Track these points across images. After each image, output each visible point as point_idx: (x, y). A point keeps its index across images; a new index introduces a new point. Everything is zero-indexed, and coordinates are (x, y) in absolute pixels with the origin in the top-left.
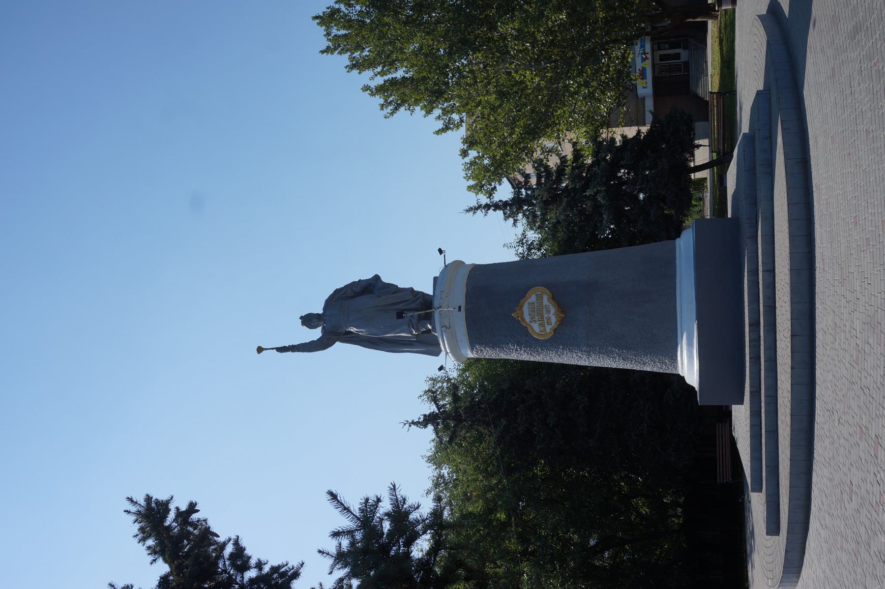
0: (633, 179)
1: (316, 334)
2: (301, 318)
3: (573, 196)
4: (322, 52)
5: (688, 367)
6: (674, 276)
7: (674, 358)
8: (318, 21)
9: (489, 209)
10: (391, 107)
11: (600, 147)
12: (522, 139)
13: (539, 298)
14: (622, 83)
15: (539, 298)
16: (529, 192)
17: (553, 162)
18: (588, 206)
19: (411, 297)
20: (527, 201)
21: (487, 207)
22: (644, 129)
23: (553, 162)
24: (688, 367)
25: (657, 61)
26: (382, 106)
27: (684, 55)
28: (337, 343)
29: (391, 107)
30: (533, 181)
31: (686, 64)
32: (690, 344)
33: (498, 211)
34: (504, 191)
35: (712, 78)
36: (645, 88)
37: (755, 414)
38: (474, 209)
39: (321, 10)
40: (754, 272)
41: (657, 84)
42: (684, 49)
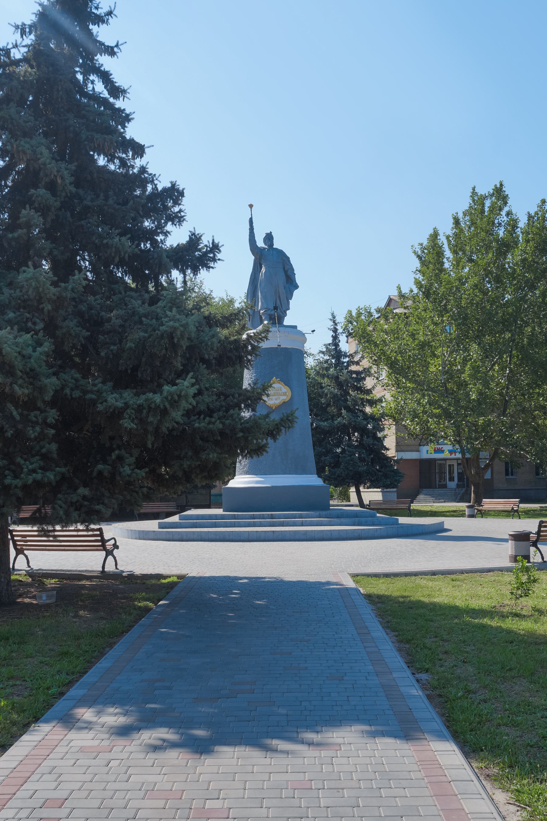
0: (353, 445)
1: (260, 243)
2: (271, 233)
3: (340, 400)
4: (474, 189)
5: (240, 481)
6: (296, 473)
7: (248, 473)
8: (498, 186)
9: (333, 331)
10: (419, 253)
11: (376, 420)
12: (388, 358)
13: (285, 394)
14: (427, 436)
15: (285, 394)
16: (345, 364)
17: (369, 383)
18: (333, 410)
19: (284, 309)
20: (339, 363)
21: (335, 330)
22: (391, 453)
23: (369, 383)
24: (240, 481)
25: (448, 463)
26: (422, 244)
27: (452, 485)
28: (254, 257)
29: (419, 253)
30: (353, 368)
31: (445, 486)
32: (257, 482)
33: (332, 339)
34: (346, 346)
35: (430, 506)
36: (427, 452)
37: (222, 517)
38: (333, 319)
39: (507, 190)
40: (301, 517)
41: (430, 462)
42: (458, 485)
